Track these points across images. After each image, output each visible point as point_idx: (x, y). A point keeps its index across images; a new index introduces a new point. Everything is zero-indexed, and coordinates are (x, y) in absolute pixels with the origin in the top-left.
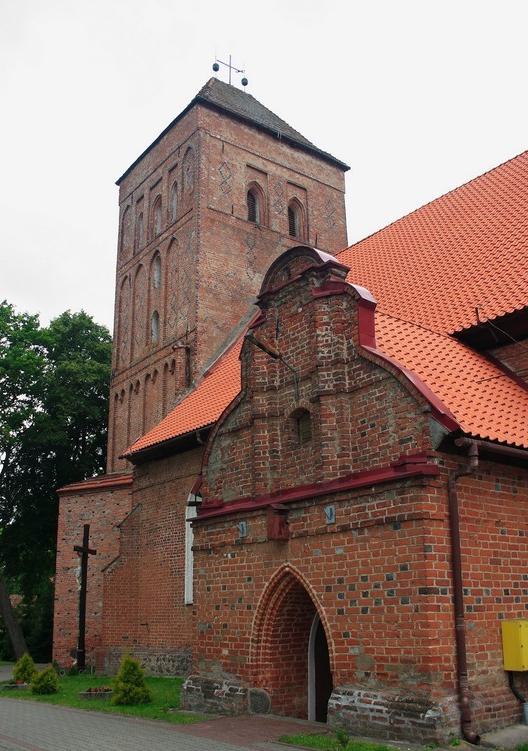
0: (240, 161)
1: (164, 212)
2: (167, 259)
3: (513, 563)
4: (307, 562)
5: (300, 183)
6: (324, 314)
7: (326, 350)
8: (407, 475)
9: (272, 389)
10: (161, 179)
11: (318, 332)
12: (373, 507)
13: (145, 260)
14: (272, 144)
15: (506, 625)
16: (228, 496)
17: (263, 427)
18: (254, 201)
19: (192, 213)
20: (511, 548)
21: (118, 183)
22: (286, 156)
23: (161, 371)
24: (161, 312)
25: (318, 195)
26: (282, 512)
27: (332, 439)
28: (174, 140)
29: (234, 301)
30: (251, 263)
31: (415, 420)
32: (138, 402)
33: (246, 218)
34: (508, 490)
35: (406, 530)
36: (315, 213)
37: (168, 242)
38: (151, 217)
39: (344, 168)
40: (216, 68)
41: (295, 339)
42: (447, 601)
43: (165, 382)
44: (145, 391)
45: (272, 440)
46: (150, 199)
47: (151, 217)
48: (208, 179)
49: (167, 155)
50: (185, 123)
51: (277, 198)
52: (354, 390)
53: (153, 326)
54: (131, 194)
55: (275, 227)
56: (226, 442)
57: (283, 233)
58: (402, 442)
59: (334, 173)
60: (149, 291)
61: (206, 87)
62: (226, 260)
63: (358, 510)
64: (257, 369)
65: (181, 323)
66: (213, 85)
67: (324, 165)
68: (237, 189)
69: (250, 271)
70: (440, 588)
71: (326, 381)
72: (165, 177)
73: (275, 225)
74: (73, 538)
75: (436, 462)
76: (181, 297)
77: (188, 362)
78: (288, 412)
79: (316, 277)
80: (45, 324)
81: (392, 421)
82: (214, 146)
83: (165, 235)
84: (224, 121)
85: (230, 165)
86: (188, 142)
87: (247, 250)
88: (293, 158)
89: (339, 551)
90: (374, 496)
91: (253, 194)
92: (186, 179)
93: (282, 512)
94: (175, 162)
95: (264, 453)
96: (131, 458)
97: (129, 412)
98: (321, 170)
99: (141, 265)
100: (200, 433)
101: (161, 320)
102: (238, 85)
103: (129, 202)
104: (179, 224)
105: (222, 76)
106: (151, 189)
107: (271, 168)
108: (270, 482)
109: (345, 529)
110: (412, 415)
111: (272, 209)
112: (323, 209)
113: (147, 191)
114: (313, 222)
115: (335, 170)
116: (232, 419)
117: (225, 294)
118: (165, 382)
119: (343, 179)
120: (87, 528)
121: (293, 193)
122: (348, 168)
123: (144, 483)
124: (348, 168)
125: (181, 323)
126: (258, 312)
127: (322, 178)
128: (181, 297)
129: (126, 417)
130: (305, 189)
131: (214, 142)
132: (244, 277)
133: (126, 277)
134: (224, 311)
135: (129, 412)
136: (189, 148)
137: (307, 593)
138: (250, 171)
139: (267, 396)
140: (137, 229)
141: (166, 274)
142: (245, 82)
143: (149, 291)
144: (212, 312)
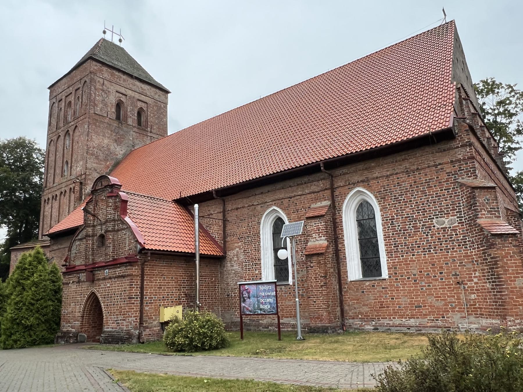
1: (73, 111)
2: (73, 135)
3: (167, 288)
4: (99, 288)
5: (144, 100)
6: (110, 202)
7: (110, 216)
8: (130, 262)
10: (71, 93)
12: (119, 271)
13: (62, 134)
14: (130, 81)
15: (181, 306)
16: (78, 263)
17: (89, 240)
18: (120, 108)
19: (85, 116)
20: (167, 283)
23: (68, 191)
24: (69, 162)
25: (153, 106)
26: (92, 271)
27: (110, 247)
28: (78, 75)
30: (116, 141)
32: (56, 204)
33: (114, 118)
34: (169, 264)
35: (126, 279)
36: (152, 115)
37: (73, 127)
38: (66, 112)
39: (167, 92)
40: (104, 32)
42: (138, 301)
43: (70, 196)
44: (60, 200)
45: (93, 244)
46: (65, 102)
47: (66, 112)
48: (95, 98)
52: (118, 230)
53: (65, 168)
54: (56, 96)
56: (78, 243)
57: (134, 125)
58: (129, 250)
60: (64, 150)
61: (97, 46)
62: (103, 139)
63: (114, 272)
66: (103, 45)
67: (157, 91)
68: (111, 103)
73: (130, 121)
77: (81, 189)
78: (98, 235)
81: (127, 243)
82: (99, 81)
83: (72, 123)
84: (105, 69)
85: (110, 90)
86: (85, 78)
89: (109, 285)
90: (119, 267)
91: (119, 105)
92: (84, 97)
93: (92, 271)
94: (79, 86)
96: (50, 235)
97: (52, 210)
99: (60, 136)
101: (69, 166)
102: (118, 43)
103: (54, 100)
104: (79, 119)
105: (108, 37)
106: (66, 97)
107: (129, 93)
109: (110, 278)
111: (129, 113)
113: (64, 97)
114: (150, 119)
115: (163, 93)
116: (80, 235)
118: (70, 196)
119: (167, 98)
121: (140, 104)
123: (55, 247)
128: (79, 157)
129: (50, 211)
130: (146, 103)
131: (99, 79)
132: (112, 148)
133: (52, 140)
134: (101, 164)
135: (52, 210)
136: (85, 81)
139: (92, 228)
140: (58, 116)
141: (73, 143)
143: (64, 150)
144: (94, 165)
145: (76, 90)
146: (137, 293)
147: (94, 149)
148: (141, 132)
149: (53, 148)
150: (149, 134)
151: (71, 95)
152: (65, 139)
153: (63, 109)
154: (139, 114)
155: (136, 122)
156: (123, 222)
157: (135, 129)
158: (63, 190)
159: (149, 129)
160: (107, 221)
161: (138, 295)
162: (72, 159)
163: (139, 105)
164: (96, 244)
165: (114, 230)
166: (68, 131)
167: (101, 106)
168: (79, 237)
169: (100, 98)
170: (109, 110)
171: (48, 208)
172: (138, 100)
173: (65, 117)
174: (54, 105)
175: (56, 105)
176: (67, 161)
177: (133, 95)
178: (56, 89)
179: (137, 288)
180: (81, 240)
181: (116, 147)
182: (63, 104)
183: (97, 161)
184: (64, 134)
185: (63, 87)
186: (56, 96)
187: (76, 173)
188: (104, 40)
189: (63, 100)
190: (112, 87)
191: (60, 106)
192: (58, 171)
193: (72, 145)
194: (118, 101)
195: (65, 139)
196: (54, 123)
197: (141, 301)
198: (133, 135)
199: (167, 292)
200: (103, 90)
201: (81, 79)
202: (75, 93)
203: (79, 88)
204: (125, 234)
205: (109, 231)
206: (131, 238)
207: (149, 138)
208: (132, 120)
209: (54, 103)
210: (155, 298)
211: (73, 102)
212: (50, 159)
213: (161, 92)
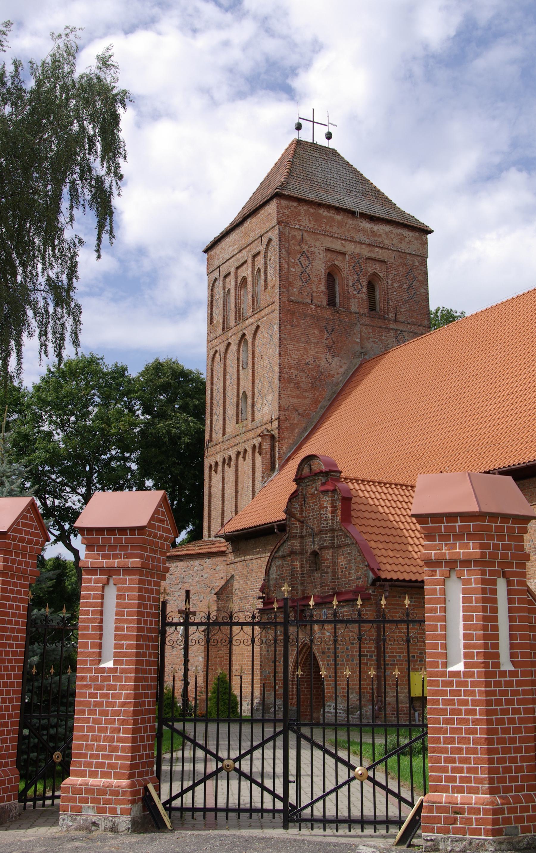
0: (318, 246)
7: (325, 523)
9: (302, 537)
10: (245, 262)
11: (322, 512)
13: (234, 341)
17: (296, 559)
18: (334, 281)
21: (206, 251)
22: (364, 231)
23: (250, 451)
25: (398, 266)
27: (327, 573)
29: (313, 387)
30: (329, 348)
31: (362, 568)
32: (230, 473)
33: (325, 303)
37: (254, 328)
39: (427, 231)
40: (299, 127)
41: (313, 509)
42: (373, 660)
46: (236, 278)
49: (251, 239)
50: (266, 213)
51: (355, 277)
52: (339, 547)
54: (219, 267)
55: (354, 308)
57: (362, 311)
58: (357, 579)
59: (417, 239)
60: (238, 371)
62: (306, 349)
64: (293, 524)
65: (266, 409)
67: (405, 232)
69: (329, 356)
70: (369, 654)
71: (325, 540)
72: (250, 261)
74: (174, 599)
75: (370, 591)
76: (266, 385)
78: (309, 551)
79: (323, 476)
80: (133, 372)
81: (353, 567)
82: (294, 237)
83: (251, 320)
84: (303, 209)
86: (269, 234)
87: (326, 337)
88: (373, 232)
91: (331, 277)
94: (258, 249)
95: (297, 574)
98: (402, 239)
100: (277, 525)
101: (250, 402)
103: (216, 274)
105: (305, 136)
107: (350, 248)
108: (300, 592)
110: (361, 566)
111: (351, 289)
112: (403, 279)
113: (233, 270)
115: (417, 234)
117: (305, 381)
120: (188, 593)
121: (371, 268)
122: (431, 232)
124: (431, 232)
125: (266, 409)
126: (293, 487)
127: (403, 246)
132: (323, 363)
133: (216, 351)
134: (305, 398)
136: (270, 240)
137: (314, 655)
138: (329, 255)
142: (329, 136)
143: (238, 371)
144: (294, 401)
145: (254, 256)
146: (371, 648)
147: (292, 371)
148: (378, 322)
149: (218, 367)
150: (392, 326)
151: (245, 266)
152: (239, 350)
153: (233, 291)
154: (371, 287)
155: (366, 304)
156: (346, 534)
157: (364, 320)
158: (241, 449)
159: (391, 315)
160: (321, 532)
161: (373, 652)
162: (253, 389)
163: (370, 269)
164: (307, 566)
165: (332, 546)
166: (244, 335)
167: (300, 283)
168: (280, 553)
169: (299, 269)
170: (315, 289)
171: (216, 479)
172: (369, 259)
173: (237, 306)
174: (217, 283)
175: (219, 284)
176: (244, 393)
177: (357, 251)
178: (218, 253)
179: (370, 640)
180: (283, 557)
181: (330, 360)
182: (233, 283)
183: (298, 392)
184: (237, 342)
185: (231, 249)
186: (219, 267)
187: (263, 416)
188: (299, 143)
189: (233, 274)
190: (318, 244)
191: (228, 286)
192: (231, 411)
193: (253, 363)
194: (329, 268)
195: (239, 350)
196: (218, 318)
197: (377, 660)
198: (361, 332)
199: (419, 649)
200: (302, 253)
201: (262, 236)
202: (253, 262)
203: (259, 253)
204: (349, 554)
205: (326, 548)
206: (358, 559)
207: (392, 333)
208: (357, 303)
209: (216, 279)
210: (400, 657)
211: (249, 279)
212: (215, 387)
213: (411, 234)
